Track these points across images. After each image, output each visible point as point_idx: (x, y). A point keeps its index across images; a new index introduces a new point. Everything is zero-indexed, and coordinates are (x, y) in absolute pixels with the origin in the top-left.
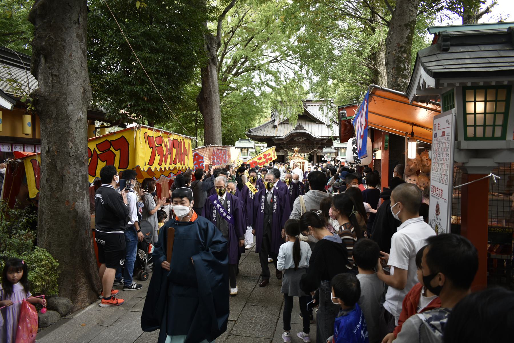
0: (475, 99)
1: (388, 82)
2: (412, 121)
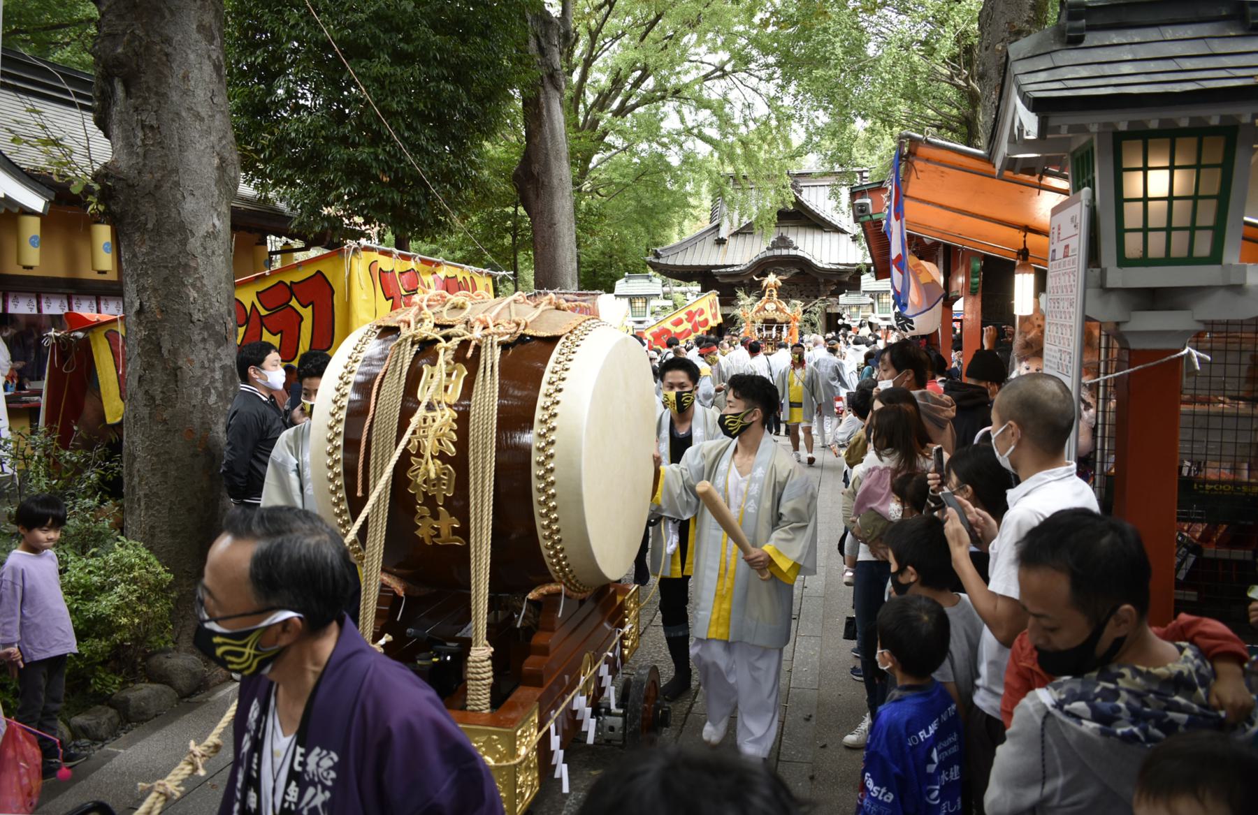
0: (1145, 161)
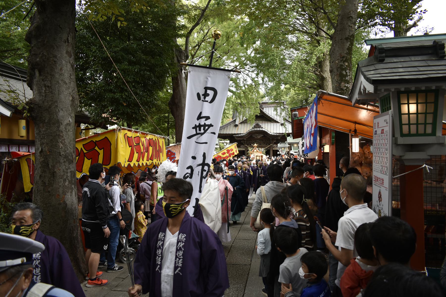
0: (408, 101)
1: (333, 87)
2: (354, 120)
